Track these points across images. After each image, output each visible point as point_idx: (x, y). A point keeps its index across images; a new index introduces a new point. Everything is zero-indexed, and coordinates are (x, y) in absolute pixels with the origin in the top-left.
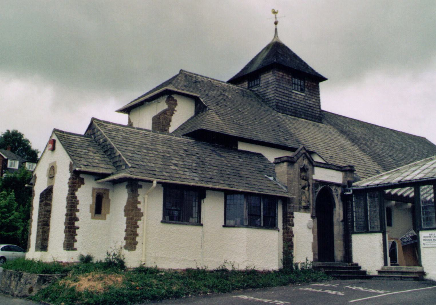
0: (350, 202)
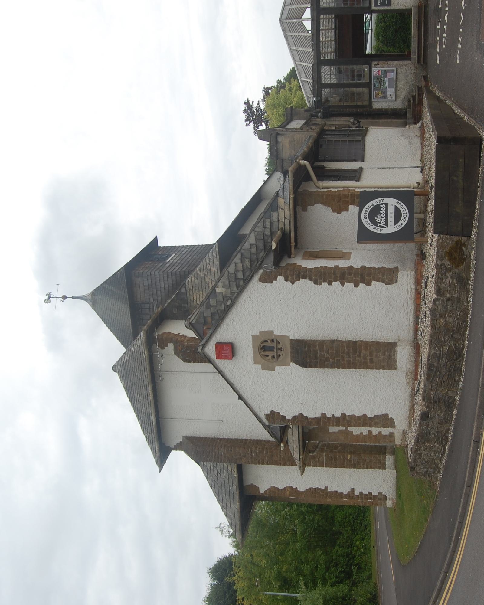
0: (331, 109)
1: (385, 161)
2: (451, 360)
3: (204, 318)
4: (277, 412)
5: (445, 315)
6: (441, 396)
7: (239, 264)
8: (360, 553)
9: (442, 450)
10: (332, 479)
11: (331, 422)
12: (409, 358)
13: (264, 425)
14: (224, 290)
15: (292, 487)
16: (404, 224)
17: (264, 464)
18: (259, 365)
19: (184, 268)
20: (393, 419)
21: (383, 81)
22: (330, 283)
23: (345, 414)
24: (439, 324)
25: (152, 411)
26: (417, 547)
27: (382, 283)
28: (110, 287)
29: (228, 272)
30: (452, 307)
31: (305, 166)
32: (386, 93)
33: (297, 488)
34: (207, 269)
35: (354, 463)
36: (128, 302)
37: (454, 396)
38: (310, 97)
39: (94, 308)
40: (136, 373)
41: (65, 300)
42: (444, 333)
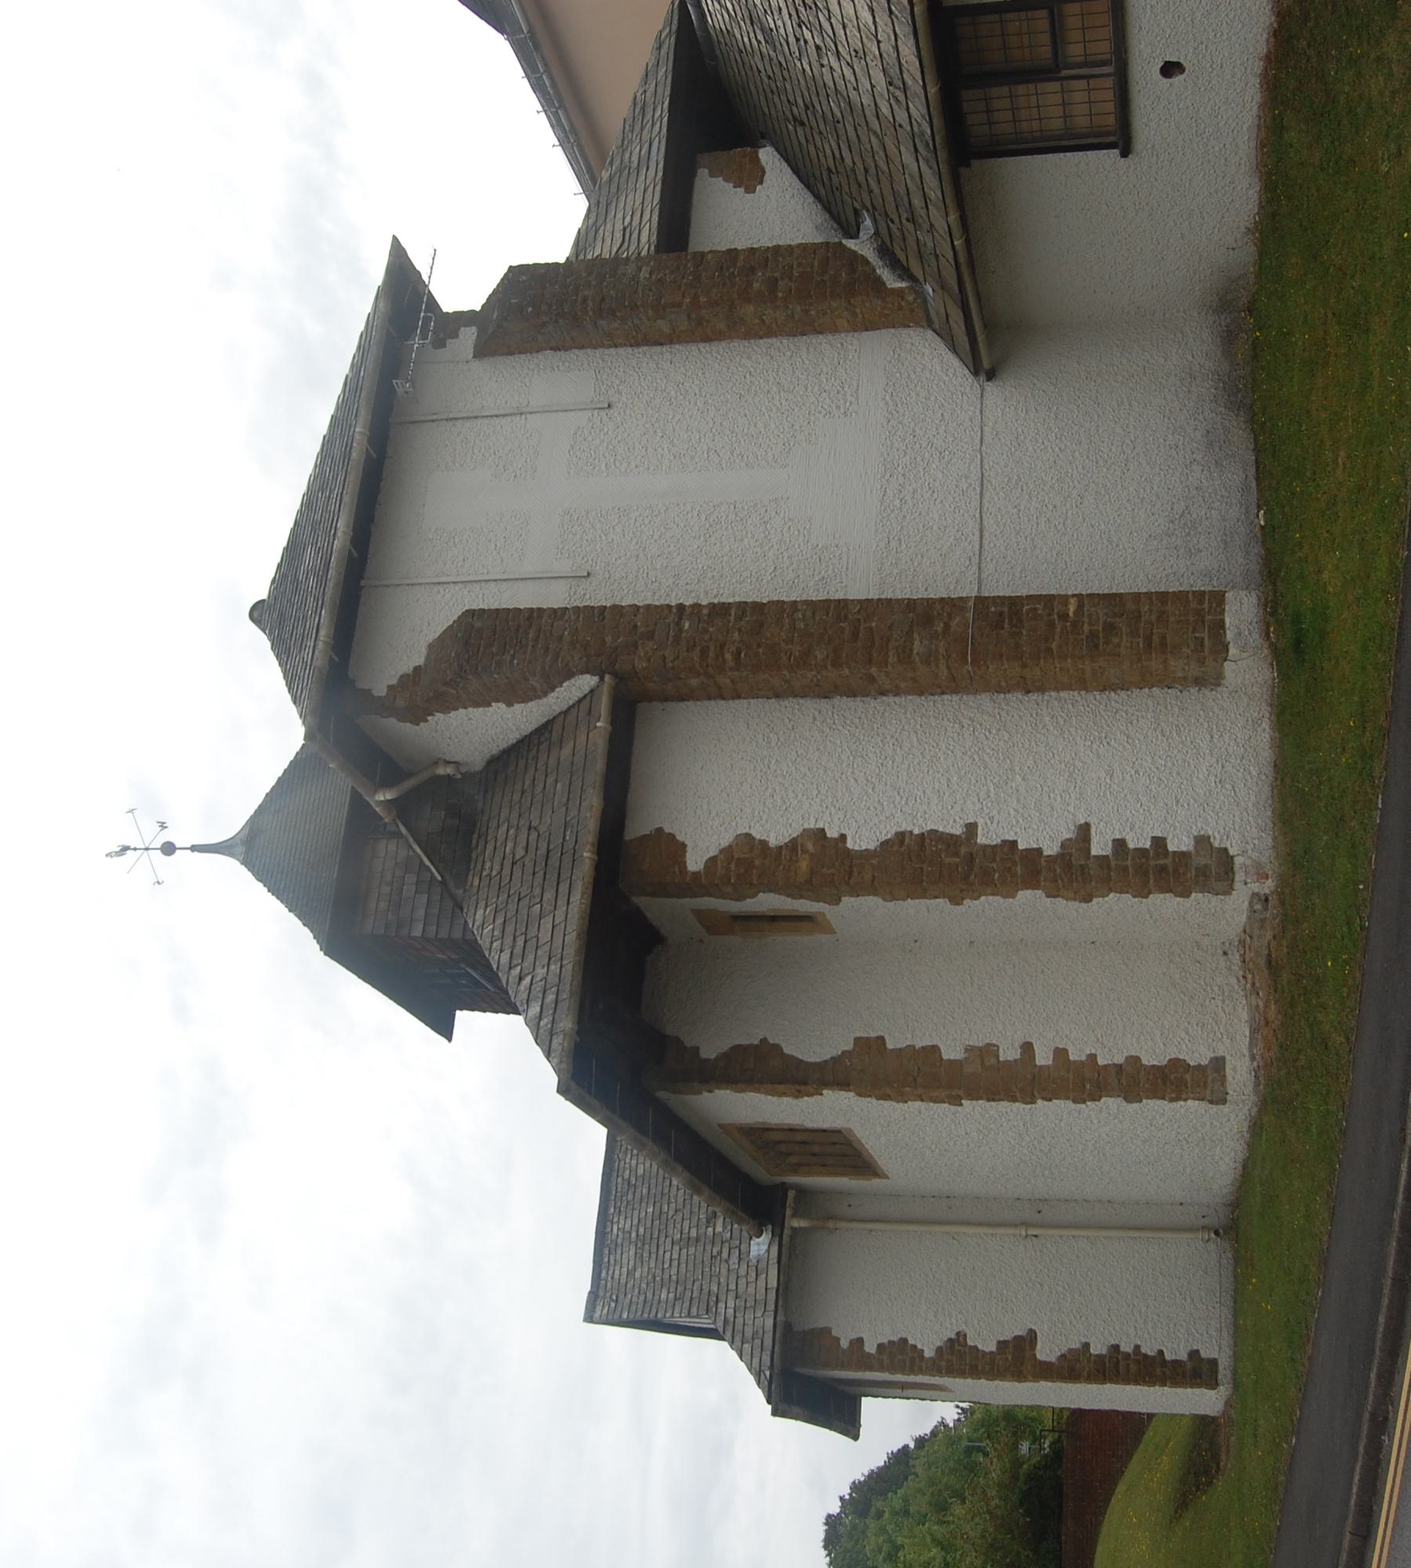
10: (996, 786)
33: (843, 837)
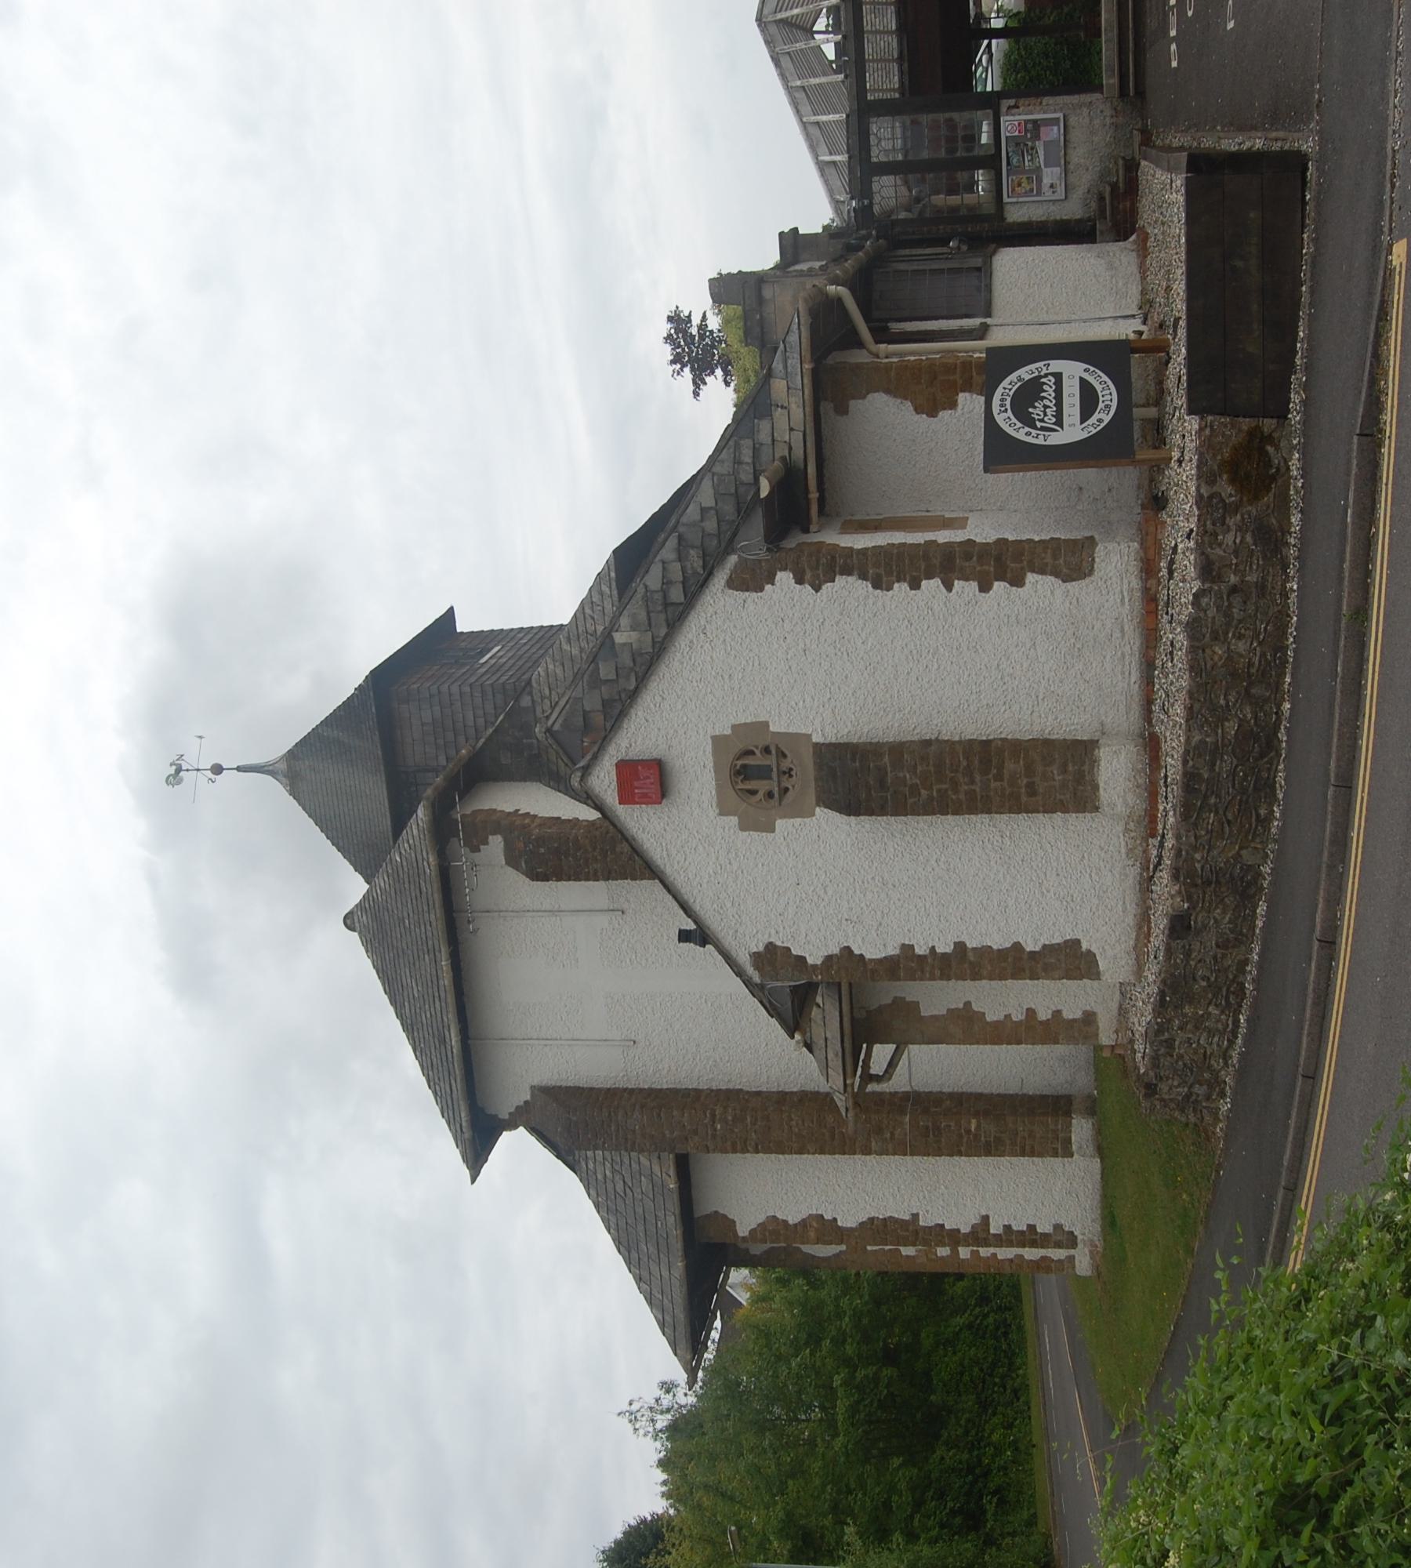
1: (1047, 312)
2: (1245, 759)
3: (585, 714)
4: (784, 947)
5: (1227, 633)
6: (1222, 865)
7: (674, 564)
8: (1002, 1462)
9: (1228, 1025)
10: (929, 1192)
11: (928, 969)
12: (1133, 779)
13: (748, 983)
14: (634, 635)
15: (822, 1216)
16: (1107, 419)
17: (748, 1152)
18: (732, 817)
19: (524, 674)
20: (1095, 955)
21: (1032, 148)
22: (915, 585)
23: (966, 945)
24: (1212, 659)
25: (450, 1016)
26: (1166, 1344)
27: (1052, 578)
28: (335, 732)
29: (646, 586)
30: (1244, 611)
31: (839, 300)
32: (1039, 180)
33: (835, 1220)
34: (587, 633)
35: (986, 1141)
36: (382, 768)
37: (1258, 862)
38: (843, 202)
39: (294, 793)
40: (407, 921)
41: (218, 777)
42: (1224, 682)
